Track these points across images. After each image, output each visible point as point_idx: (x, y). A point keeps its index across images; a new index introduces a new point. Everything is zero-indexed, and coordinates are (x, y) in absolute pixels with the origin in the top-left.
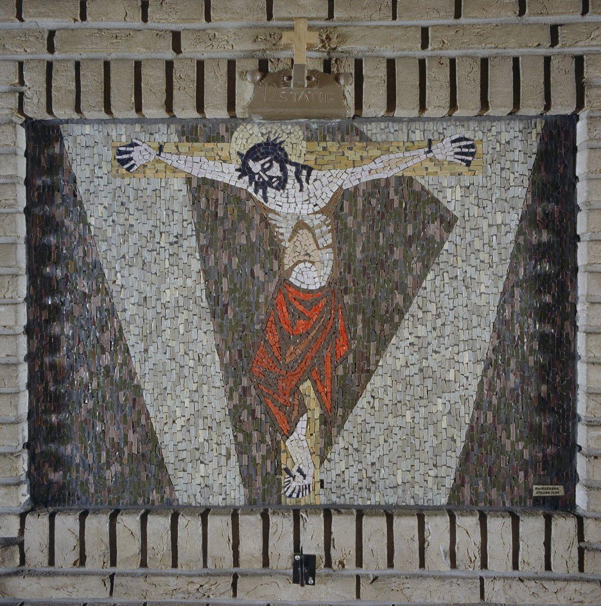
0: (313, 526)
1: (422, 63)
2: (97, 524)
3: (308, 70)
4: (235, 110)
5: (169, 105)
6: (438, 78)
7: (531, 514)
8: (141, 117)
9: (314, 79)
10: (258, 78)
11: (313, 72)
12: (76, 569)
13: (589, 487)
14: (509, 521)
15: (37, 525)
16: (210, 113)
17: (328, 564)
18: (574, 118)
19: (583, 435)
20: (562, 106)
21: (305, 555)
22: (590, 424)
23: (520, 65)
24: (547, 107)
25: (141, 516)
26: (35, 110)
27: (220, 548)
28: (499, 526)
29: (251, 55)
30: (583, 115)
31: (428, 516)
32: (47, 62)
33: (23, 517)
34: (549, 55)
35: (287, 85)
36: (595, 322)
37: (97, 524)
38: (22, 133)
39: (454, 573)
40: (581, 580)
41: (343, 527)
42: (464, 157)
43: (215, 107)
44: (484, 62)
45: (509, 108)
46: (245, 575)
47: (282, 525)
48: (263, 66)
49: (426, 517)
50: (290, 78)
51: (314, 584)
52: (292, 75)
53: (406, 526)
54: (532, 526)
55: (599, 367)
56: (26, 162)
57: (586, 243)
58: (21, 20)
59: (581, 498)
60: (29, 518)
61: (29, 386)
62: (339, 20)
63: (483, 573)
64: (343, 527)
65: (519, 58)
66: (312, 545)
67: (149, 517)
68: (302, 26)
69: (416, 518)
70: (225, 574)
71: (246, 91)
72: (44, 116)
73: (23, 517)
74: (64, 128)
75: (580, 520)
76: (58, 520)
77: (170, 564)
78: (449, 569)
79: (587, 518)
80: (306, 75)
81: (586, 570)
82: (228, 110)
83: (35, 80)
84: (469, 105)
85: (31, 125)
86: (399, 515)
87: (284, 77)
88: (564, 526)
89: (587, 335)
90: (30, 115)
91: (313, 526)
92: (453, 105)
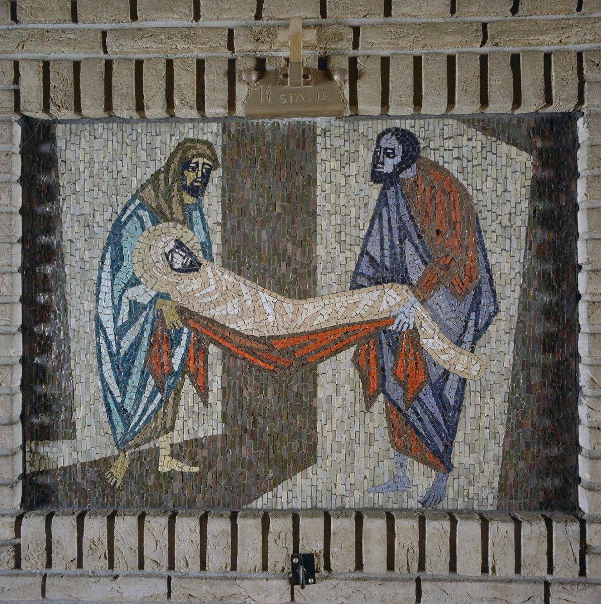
3: (304, 68)
6: (123, 79)
10: (254, 78)
11: (307, 70)
13: (592, 458)
15: (33, 525)
17: (327, 567)
18: (566, 122)
19: (584, 469)
20: (562, 104)
21: (304, 555)
22: (590, 488)
23: (521, 66)
24: (549, 101)
26: (33, 108)
33: (19, 519)
34: (516, 52)
35: (284, 84)
36: (596, 417)
37: (187, 527)
38: (18, 130)
41: (343, 526)
42: (147, 394)
45: (473, 103)
50: (286, 76)
51: (314, 583)
54: (218, 526)
57: (586, 273)
58: (17, 22)
59: (584, 501)
61: (22, 387)
63: (549, 578)
65: (421, 56)
71: (242, 91)
72: (41, 116)
74: (59, 130)
75: (583, 523)
80: (302, 74)
85: (27, 123)
90: (26, 114)
91: (311, 529)
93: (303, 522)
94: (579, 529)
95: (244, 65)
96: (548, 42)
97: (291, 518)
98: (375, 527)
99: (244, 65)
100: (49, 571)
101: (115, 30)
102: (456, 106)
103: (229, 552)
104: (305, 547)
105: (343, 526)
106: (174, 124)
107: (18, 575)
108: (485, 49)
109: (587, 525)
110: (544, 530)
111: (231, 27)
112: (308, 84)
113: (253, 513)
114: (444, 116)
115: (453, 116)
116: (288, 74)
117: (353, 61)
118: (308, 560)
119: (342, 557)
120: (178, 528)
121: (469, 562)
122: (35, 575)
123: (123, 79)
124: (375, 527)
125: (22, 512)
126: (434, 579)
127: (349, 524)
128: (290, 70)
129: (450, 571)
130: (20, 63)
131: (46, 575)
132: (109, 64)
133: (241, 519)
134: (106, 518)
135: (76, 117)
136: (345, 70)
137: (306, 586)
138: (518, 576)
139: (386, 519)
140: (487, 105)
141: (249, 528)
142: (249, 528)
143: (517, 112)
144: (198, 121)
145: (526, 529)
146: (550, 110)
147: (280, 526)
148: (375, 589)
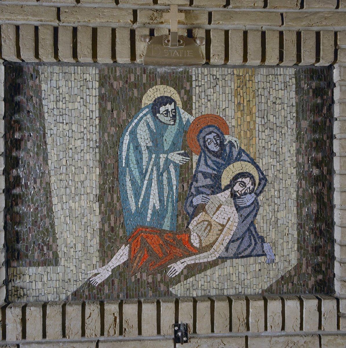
0: (186, 308)
1: (281, 33)
2: (274, 306)
4: (97, 58)
5: (95, 55)
6: (65, 39)
7: (290, 299)
9: (166, 41)
11: (181, 37)
14: (316, 302)
17: (195, 331)
18: (330, 68)
24: (318, 60)
26: (9, 55)
30: (336, 66)
31: (324, 299)
33: (64, 307)
34: (37, 25)
35: (167, 45)
37: (149, 309)
39: (64, 339)
40: (46, 343)
41: (203, 307)
43: (85, 56)
44: (36, 28)
47: (168, 309)
49: (216, 302)
50: (168, 41)
51: (186, 342)
53: (221, 307)
55: (345, 211)
59: (337, 286)
60: (8, 311)
63: (320, 332)
65: (210, 30)
66: (185, 318)
68: (174, 9)
71: (141, 47)
72: (14, 59)
75: (338, 300)
77: (137, 332)
79: (343, 299)
82: (92, 58)
85: (8, 66)
87: (160, 40)
88: (328, 305)
89: (341, 193)
90: (7, 58)
91: (186, 308)
92: (281, 59)
93: (251, 303)
94: (209, 306)
95: (142, 32)
99: (142, 32)
100: (102, 339)
101: (36, 6)
102: (229, 61)
105: (203, 307)
107: (121, 341)
108: (282, 29)
109: (340, 301)
110: (281, 305)
112: (180, 45)
114: (260, 66)
116: (169, 40)
117: (208, 32)
119: (203, 325)
120: (48, 312)
122: (92, 342)
123: (65, 39)
124: (221, 307)
127: (59, 309)
130: (98, 30)
131: (98, 341)
133: (69, 306)
136: (204, 38)
138: (302, 331)
139: (137, 304)
140: (247, 61)
143: (317, 65)
144: (73, 65)
145: (163, 305)
147: (168, 309)
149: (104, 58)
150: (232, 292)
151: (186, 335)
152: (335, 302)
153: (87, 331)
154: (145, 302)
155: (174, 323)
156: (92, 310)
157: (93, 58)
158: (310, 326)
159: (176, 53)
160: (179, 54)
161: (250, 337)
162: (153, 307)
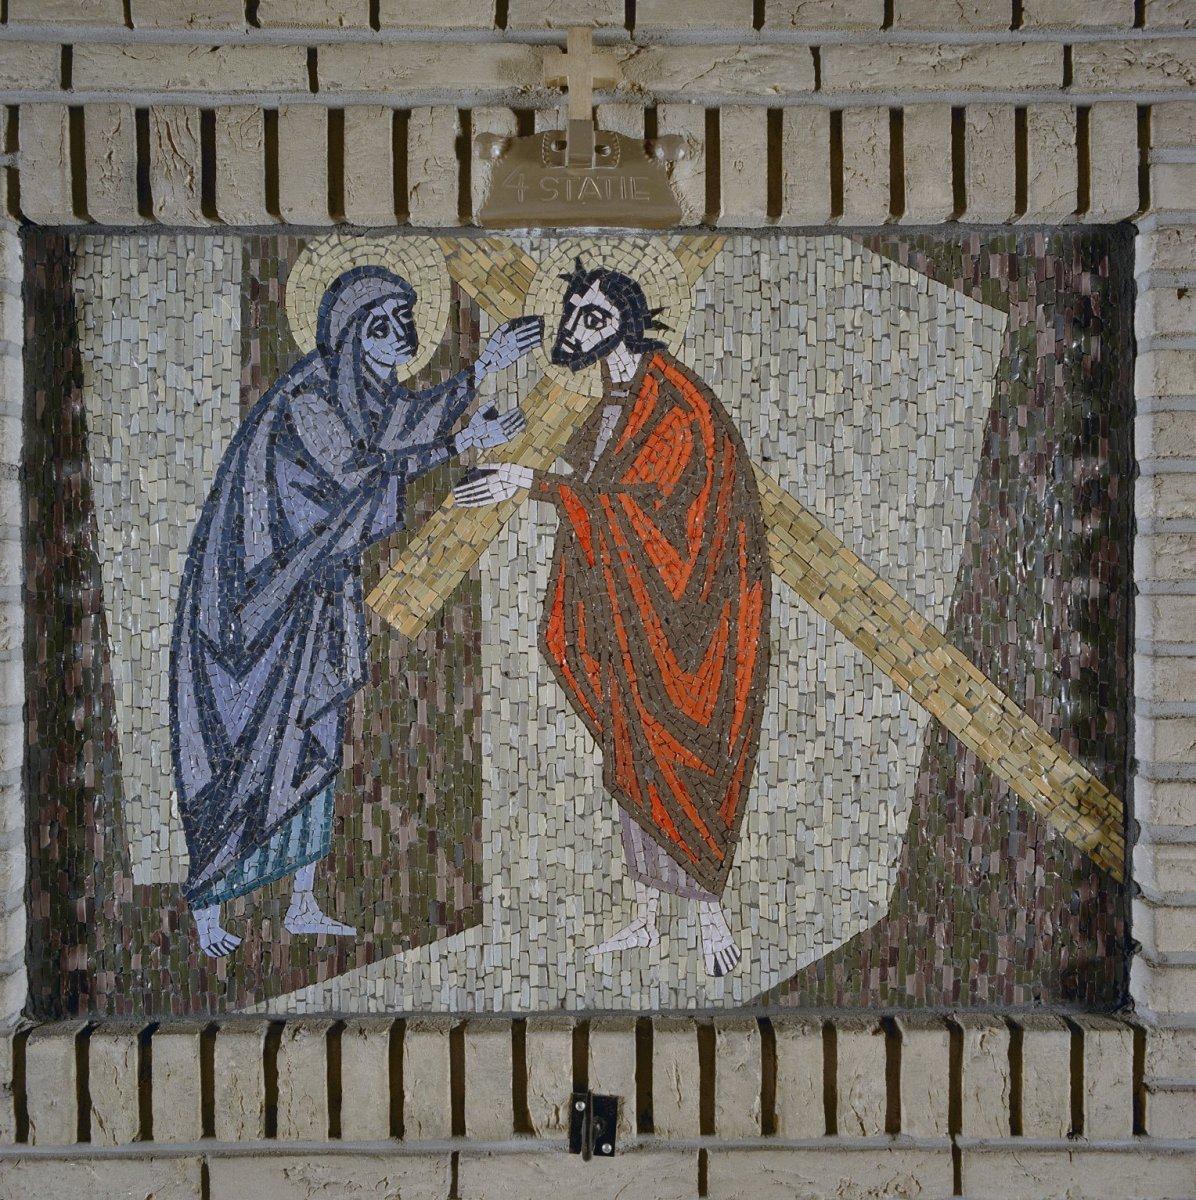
4: (344, 214)
6: (368, 145)
8: (216, 224)
9: (553, 147)
10: (497, 153)
12: (1066, 1142)
14: (1065, 1039)
16: (910, 216)
17: (646, 1122)
18: (1125, 231)
20: (1112, 201)
25: (328, 1034)
26: (47, 202)
27: (427, 1096)
28: (926, 1049)
29: (500, 100)
32: (266, 111)
38: (15, 248)
41: (676, 1053)
46: (476, 1154)
48: (525, 119)
50: (562, 145)
51: (612, 1154)
52: (567, 139)
54: (176, 1052)
56: (1136, 322)
60: (35, 1049)
62: (1159, 29)
64: (676, 1053)
67: (469, 1040)
69: (693, 1036)
70: (691, 1151)
71: (481, 172)
73: (20, 1041)
76: (159, 1043)
78: (327, 1140)
81: (345, 1133)
83: (44, 138)
84: (369, 202)
85: (29, 231)
86: (846, 1029)
88: (1109, 1050)
93: (533, 1040)
96: (957, 86)
97: (324, 1035)
98: (488, 1053)
102: (906, 213)
103: (1086, 1084)
104: (601, 1083)
106: (773, 238)
111: (312, 44)
113: (245, 1027)
115: (848, 232)
118: (607, 1108)
120: (282, 1062)
121: (802, 1112)
123: (368, 145)
124: (488, 1053)
125: (28, 1024)
126: (985, 1149)
127: (501, 1044)
128: (590, 138)
129: (702, 1133)
132: (77, 114)
134: (198, 1036)
135: (205, 223)
137: (595, 1158)
141: (239, 1057)
142: (239, 1057)
143: (1020, 222)
145: (972, 1039)
146: (1088, 219)
148: (360, 1171)
149: (241, 202)
150: (527, 1000)
151: (610, 1138)
152: (1129, 1038)
153: (720, 1120)
154: (912, 1026)
155: (570, 1089)
156: (800, 1054)
157: (397, 212)
158: (923, 1115)
159: (590, 187)
160: (601, 187)
161: (714, 1151)
162: (815, 1044)
